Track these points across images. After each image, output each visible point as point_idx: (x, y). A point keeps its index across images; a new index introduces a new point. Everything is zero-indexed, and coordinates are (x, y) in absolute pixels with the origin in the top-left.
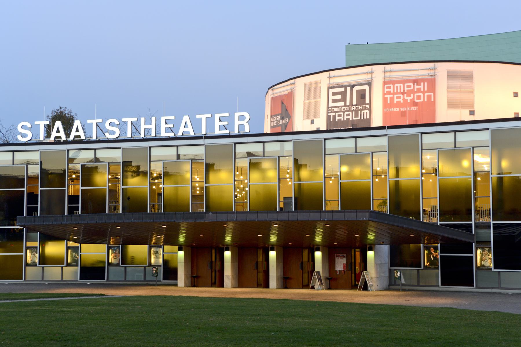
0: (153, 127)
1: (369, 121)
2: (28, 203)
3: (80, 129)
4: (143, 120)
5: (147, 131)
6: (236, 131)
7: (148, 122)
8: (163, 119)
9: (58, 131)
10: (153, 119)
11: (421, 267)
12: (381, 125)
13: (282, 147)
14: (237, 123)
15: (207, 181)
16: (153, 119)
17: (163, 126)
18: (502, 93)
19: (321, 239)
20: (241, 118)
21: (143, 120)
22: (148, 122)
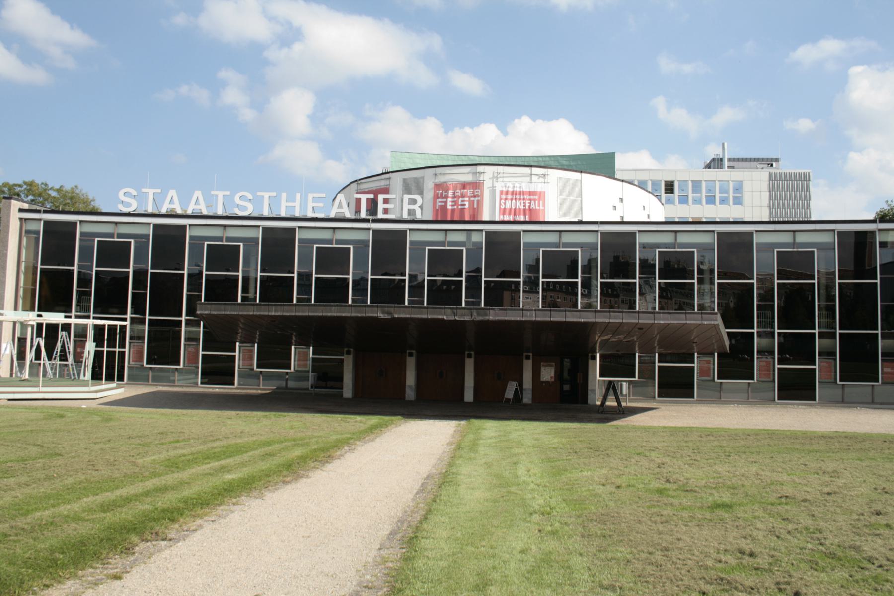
0: (297, 204)
1: (476, 209)
2: (133, 288)
3: (201, 200)
4: (284, 195)
5: (412, 212)
6: (405, 216)
7: (290, 198)
8: (311, 196)
9: (172, 201)
10: (298, 195)
11: (753, 379)
12: (430, 218)
13: (469, 238)
14: (406, 207)
15: (676, 240)
16: (298, 195)
17: (310, 205)
18: (26, 12)
19: (553, 375)
20: (412, 202)
21: (284, 195)
22: (290, 198)
